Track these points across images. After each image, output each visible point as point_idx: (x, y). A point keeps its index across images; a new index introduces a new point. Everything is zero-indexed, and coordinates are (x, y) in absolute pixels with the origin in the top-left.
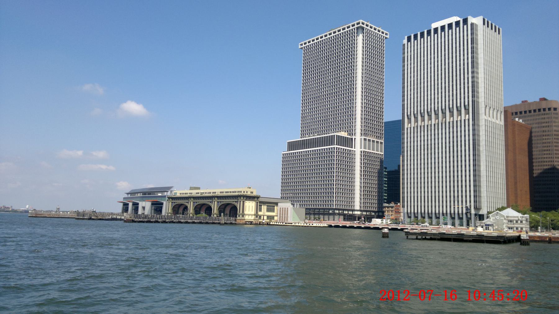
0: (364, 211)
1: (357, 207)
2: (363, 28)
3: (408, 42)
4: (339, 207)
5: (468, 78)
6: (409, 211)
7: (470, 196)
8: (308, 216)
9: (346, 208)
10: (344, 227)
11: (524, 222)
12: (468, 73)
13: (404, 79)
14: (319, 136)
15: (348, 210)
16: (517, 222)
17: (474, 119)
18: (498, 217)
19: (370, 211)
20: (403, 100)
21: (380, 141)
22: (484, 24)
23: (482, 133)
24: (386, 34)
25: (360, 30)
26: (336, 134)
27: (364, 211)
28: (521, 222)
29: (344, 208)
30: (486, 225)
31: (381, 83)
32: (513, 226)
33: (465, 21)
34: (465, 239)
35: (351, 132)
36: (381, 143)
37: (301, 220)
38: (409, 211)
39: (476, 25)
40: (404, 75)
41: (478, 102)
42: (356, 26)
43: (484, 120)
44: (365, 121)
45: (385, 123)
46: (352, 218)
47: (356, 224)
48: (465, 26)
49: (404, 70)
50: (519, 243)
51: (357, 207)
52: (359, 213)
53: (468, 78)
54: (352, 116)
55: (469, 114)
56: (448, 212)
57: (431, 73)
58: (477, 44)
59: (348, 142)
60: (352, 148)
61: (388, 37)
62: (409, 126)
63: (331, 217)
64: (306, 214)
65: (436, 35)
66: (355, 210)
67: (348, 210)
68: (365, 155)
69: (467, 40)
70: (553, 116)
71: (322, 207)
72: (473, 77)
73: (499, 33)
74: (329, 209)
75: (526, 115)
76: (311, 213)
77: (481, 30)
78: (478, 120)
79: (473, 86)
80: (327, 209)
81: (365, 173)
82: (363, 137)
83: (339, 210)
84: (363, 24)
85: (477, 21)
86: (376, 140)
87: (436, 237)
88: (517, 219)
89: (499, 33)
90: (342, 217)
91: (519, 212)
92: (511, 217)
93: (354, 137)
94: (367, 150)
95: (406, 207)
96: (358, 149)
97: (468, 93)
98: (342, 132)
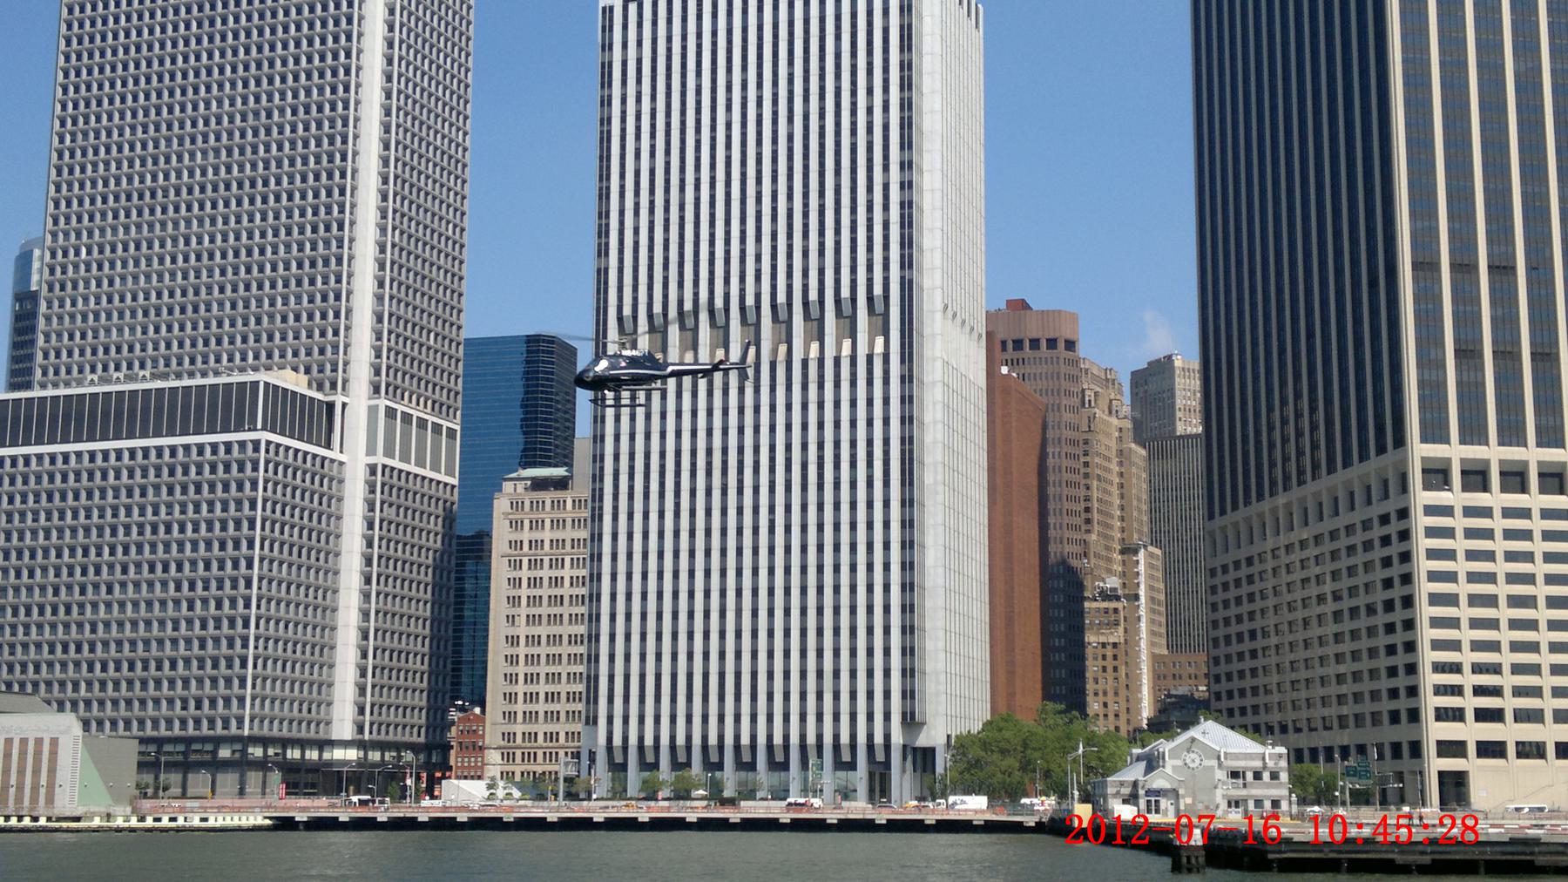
1: (343, 728)
4: (266, 732)
5: (886, 187)
7: (887, 673)
9: (294, 734)
12: (886, 168)
13: (605, 158)
14: (159, 384)
15: (303, 744)
16: (1257, 776)
17: (907, 356)
18: (1193, 759)
19: (398, 747)
20: (603, 251)
21: (445, 424)
26: (263, 377)
27: (382, 746)
28: (1275, 776)
29: (285, 733)
30: (1149, 793)
31: (455, 166)
32: (1243, 792)
34: (1541, 860)
35: (329, 374)
36: (451, 433)
37: (117, 800)
40: (605, 138)
43: (939, 364)
44: (396, 327)
45: (469, 342)
46: (330, 780)
49: (606, 121)
50: (1166, 862)
51: (343, 728)
52: (352, 754)
53: (886, 187)
54: (334, 299)
55: (886, 334)
56: (828, 739)
57: (728, 146)
59: (318, 420)
60: (328, 446)
62: (846, 350)
63: (228, 780)
64: (142, 766)
66: (332, 744)
67: (303, 744)
68: (388, 488)
69: (886, 31)
70: (1063, 369)
71: (177, 731)
74: (218, 741)
76: (171, 760)
80: (204, 740)
81: (383, 568)
83: (265, 742)
86: (431, 419)
87: (1411, 858)
88: (1258, 764)
90: (276, 777)
91: (1257, 731)
93: (339, 399)
95: (602, 721)
96: (355, 452)
97: (886, 247)
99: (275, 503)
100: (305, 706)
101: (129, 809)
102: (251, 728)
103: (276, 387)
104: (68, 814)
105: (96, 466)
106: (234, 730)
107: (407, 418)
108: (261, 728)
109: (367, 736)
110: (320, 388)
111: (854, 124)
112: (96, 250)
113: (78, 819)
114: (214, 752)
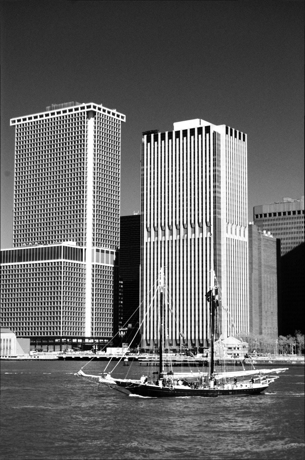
0: (96, 338)
1: (88, 334)
2: (94, 113)
3: (147, 142)
6: (148, 338)
8: (33, 346)
9: (75, 336)
10: (77, 359)
11: (240, 349)
15: (78, 338)
19: (104, 338)
22: (227, 133)
23: (223, 253)
24: (122, 117)
25: (91, 114)
27: (96, 338)
28: (238, 348)
32: (231, 352)
33: (208, 129)
37: (25, 353)
38: (148, 338)
39: (219, 135)
41: (220, 219)
42: (86, 110)
46: (85, 347)
47: (89, 354)
48: (208, 135)
58: (219, 155)
60: (82, 261)
61: (124, 120)
63: (58, 347)
64: (31, 344)
65: (178, 139)
68: (97, 269)
72: (215, 192)
73: (244, 140)
75: (285, 217)
77: (223, 138)
78: (220, 239)
79: (215, 202)
82: (95, 248)
84: (95, 107)
85: (220, 129)
89: (244, 140)
92: (230, 345)
93: (84, 248)
94: (100, 264)
96: (89, 261)
98: (69, 242)
99: (66, 277)
100: (77, 328)
101: (28, 355)
102: (63, 334)
103: (66, 247)
104: (14, 356)
105: (25, 269)
106: (58, 335)
107: (103, 251)
108: (65, 334)
109: (94, 336)
110: (79, 245)
111: (202, 176)
112: (61, 145)
113: (16, 357)
114: (54, 340)
